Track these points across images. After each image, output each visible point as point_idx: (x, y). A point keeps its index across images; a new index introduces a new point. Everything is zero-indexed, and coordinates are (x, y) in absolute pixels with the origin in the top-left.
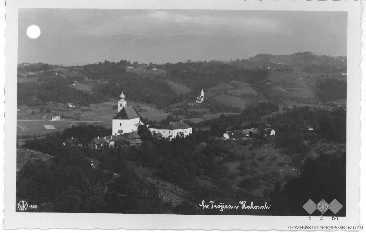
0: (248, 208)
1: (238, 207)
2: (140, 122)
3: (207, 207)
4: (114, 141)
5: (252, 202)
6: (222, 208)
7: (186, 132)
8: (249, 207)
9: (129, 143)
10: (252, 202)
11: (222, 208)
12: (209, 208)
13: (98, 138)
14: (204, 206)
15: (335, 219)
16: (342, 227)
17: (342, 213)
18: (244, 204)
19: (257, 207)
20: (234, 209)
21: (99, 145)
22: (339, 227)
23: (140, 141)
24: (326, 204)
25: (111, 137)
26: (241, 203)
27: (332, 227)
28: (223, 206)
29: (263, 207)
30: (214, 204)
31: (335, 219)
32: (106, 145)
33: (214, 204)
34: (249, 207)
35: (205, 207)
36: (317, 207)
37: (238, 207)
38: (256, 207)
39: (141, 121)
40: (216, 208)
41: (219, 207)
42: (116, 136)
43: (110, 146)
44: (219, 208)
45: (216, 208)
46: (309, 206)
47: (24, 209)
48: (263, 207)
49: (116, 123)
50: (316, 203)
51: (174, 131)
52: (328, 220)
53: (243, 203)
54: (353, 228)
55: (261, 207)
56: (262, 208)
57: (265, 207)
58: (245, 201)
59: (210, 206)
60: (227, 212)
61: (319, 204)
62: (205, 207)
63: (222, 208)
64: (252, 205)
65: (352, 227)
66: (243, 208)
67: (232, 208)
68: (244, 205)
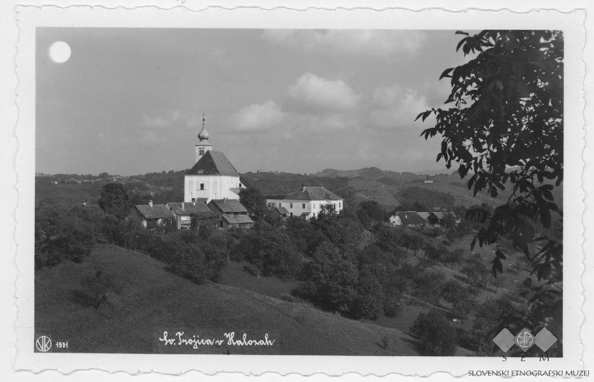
0: (239, 345)
1: (221, 341)
2: (240, 185)
3: (171, 341)
4: (190, 216)
5: (245, 335)
6: (196, 343)
7: (314, 208)
8: (239, 343)
9: (224, 223)
10: (245, 335)
11: (196, 344)
12: (175, 344)
13: (151, 204)
14: (166, 340)
15: (544, 360)
16: (555, 373)
17: (556, 351)
18: (232, 337)
19: (252, 342)
20: (216, 345)
21: (152, 221)
22: (550, 372)
23: (246, 219)
24: (531, 336)
25: (183, 205)
26: (227, 335)
27: (540, 372)
28: (198, 341)
29: (262, 342)
30: (182, 337)
31: (544, 360)
32: (171, 223)
33: (182, 337)
34: (239, 343)
35: (169, 343)
36: (534, 340)
37: (221, 341)
38: (250, 342)
39: (242, 184)
40: (187, 343)
41: (190, 342)
42: (195, 204)
43: (179, 227)
44: (191, 343)
45: (187, 343)
46: (504, 339)
47: (46, 349)
48: (262, 342)
49: (191, 183)
50: (515, 332)
51: (313, 202)
52: (533, 363)
53: (230, 336)
54: (573, 374)
55: (260, 342)
56: (261, 344)
57: (265, 341)
58: (233, 333)
59: (177, 341)
60: (203, 350)
61: (519, 336)
62: (169, 343)
63: (196, 344)
64: (244, 339)
65: (571, 372)
66: (230, 344)
67: (212, 344)
68: (231, 339)
